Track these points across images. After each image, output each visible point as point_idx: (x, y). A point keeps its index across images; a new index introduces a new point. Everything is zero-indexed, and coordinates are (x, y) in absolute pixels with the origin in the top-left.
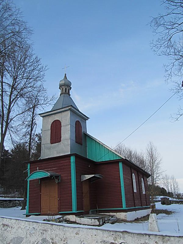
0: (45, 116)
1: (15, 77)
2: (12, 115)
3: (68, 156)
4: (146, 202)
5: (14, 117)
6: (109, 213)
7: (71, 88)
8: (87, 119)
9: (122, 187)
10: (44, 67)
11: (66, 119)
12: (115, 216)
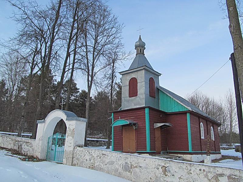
0: (123, 73)
1: (96, 36)
2: (96, 70)
3: (144, 108)
4: (215, 148)
5: (98, 72)
6: (177, 154)
7: (145, 48)
8: (160, 75)
9: (188, 135)
10: (121, 25)
11: (141, 78)
12: (182, 157)
